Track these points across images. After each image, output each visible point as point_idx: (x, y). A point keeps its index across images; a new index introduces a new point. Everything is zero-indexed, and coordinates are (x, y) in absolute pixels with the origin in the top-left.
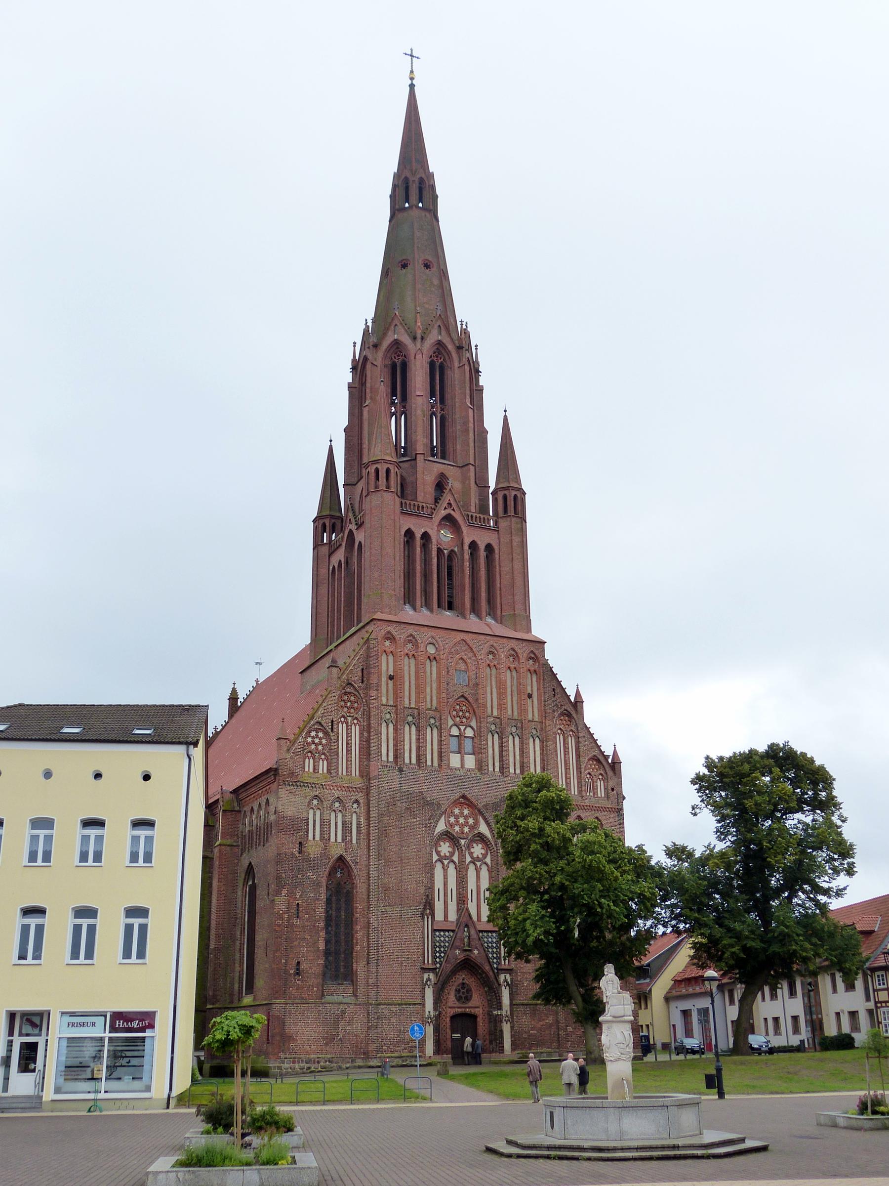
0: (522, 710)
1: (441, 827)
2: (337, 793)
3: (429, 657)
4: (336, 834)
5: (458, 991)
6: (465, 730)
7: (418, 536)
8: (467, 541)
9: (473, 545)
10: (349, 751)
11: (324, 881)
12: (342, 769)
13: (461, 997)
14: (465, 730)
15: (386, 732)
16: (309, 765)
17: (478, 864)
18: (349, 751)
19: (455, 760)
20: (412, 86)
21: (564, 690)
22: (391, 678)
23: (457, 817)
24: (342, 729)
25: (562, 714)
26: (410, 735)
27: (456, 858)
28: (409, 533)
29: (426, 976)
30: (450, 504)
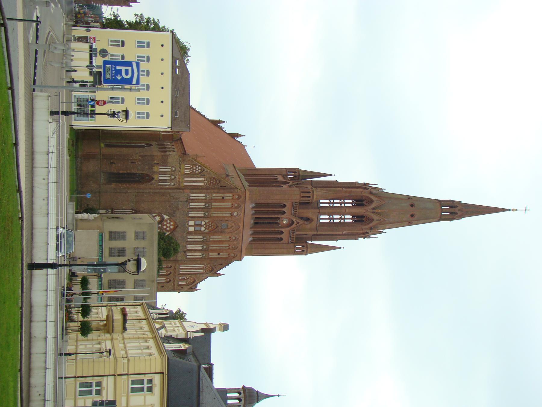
0: (213, 251)
1: (166, 217)
2: (177, 177)
6: (204, 227)
7: (283, 209)
8: (283, 230)
9: (282, 233)
10: (194, 181)
11: (144, 172)
12: (186, 179)
14: (204, 227)
15: (202, 196)
16: (188, 166)
18: (194, 181)
19: (192, 223)
20: (508, 210)
21: (222, 268)
22: (223, 198)
23: (169, 223)
24: (202, 179)
25: (212, 267)
28: (284, 206)
30: (298, 223)
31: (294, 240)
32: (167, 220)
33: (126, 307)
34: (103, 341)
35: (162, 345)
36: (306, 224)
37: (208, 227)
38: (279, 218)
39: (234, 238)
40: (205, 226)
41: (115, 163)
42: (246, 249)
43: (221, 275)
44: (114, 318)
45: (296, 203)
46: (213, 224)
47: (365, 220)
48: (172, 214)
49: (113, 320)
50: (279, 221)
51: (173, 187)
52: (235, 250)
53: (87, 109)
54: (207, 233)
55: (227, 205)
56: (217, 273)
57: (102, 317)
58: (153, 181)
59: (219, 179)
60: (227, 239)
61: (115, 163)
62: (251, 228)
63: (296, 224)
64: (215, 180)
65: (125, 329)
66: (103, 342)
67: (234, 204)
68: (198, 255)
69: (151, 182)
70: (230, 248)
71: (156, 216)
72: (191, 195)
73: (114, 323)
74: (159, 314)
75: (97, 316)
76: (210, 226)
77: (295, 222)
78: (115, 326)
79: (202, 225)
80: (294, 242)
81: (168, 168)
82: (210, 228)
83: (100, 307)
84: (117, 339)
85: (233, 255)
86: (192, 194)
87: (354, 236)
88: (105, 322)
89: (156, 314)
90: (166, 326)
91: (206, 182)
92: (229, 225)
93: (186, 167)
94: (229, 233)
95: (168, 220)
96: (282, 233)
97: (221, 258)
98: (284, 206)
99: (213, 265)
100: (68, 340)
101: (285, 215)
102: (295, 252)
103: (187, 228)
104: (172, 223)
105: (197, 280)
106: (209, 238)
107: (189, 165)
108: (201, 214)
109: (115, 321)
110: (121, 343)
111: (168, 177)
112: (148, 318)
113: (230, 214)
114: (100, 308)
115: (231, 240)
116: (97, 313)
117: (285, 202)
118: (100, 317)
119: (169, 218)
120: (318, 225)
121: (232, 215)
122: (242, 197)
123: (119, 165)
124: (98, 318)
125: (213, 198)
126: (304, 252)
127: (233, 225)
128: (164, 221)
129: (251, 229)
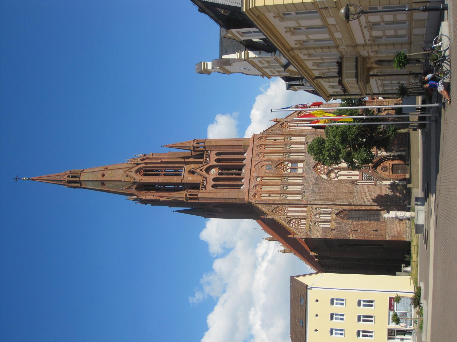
0: (280, 144)
1: (325, 177)
2: (313, 216)
3: (262, 180)
4: (328, 217)
5: (384, 171)
6: (288, 167)
7: (214, 183)
10: (297, 212)
12: (304, 214)
13: (386, 170)
14: (288, 167)
15: (291, 197)
16: (303, 227)
17: (338, 175)
18: (297, 212)
19: (300, 171)
22: (270, 195)
23: (321, 171)
24: (289, 214)
26: (291, 188)
27: (336, 171)
28: (214, 186)
29: (378, 184)
30: (201, 170)
31: (205, 154)
32: (323, 174)
33: (343, 93)
34: (370, 42)
35: (266, 35)
36: (193, 168)
37: (285, 167)
38: (220, 174)
39: (260, 156)
40: (288, 168)
41: (373, 230)
42: (250, 145)
43: (273, 121)
44: (355, 79)
45: (203, 189)
46: (280, 169)
47: (143, 172)
48: (318, 180)
49: (357, 76)
50: (219, 171)
51: (317, 207)
52: (260, 144)
53: (393, 335)
54: (285, 161)
55: (266, 189)
56: (276, 121)
57: (377, 80)
58: (336, 212)
59: (273, 213)
60: (266, 155)
61: (373, 230)
62: (244, 165)
63: (203, 168)
64: (277, 213)
65: (340, 64)
66: (369, 40)
67: (259, 189)
68: (295, 139)
69: (338, 211)
70: (264, 146)
71: (334, 178)
72: (300, 198)
73: (356, 71)
74: (300, 85)
75: (384, 82)
76: (282, 168)
77: (203, 170)
78: (354, 67)
79: (290, 169)
80: (205, 152)
81: (322, 225)
82: (283, 165)
83: (381, 92)
84: (347, 46)
85: (262, 139)
86: (299, 199)
87: (154, 157)
88: (371, 73)
89: (303, 85)
90: (283, 69)
91: (286, 211)
92: (265, 169)
93: (305, 226)
94: (265, 161)
95: (323, 174)
96: (217, 161)
97: (272, 137)
98: (214, 186)
99: (280, 129)
100: (424, 44)
101: (212, 178)
102: (204, 142)
103: (305, 165)
104: (319, 170)
105: (296, 115)
106: (284, 156)
107: (302, 228)
108: (291, 180)
109: (354, 75)
110: (339, 39)
111: (322, 217)
112: (313, 80)
113: (263, 180)
114: (382, 91)
115: (262, 154)
116: (384, 85)
117: (213, 190)
118: (379, 81)
119: (321, 176)
120: (184, 167)
121: (262, 178)
122: (251, 196)
123: (369, 229)
124: (382, 80)
125: (279, 195)
126: (196, 142)
127: (261, 169)
128: (327, 173)
129: (244, 164)
